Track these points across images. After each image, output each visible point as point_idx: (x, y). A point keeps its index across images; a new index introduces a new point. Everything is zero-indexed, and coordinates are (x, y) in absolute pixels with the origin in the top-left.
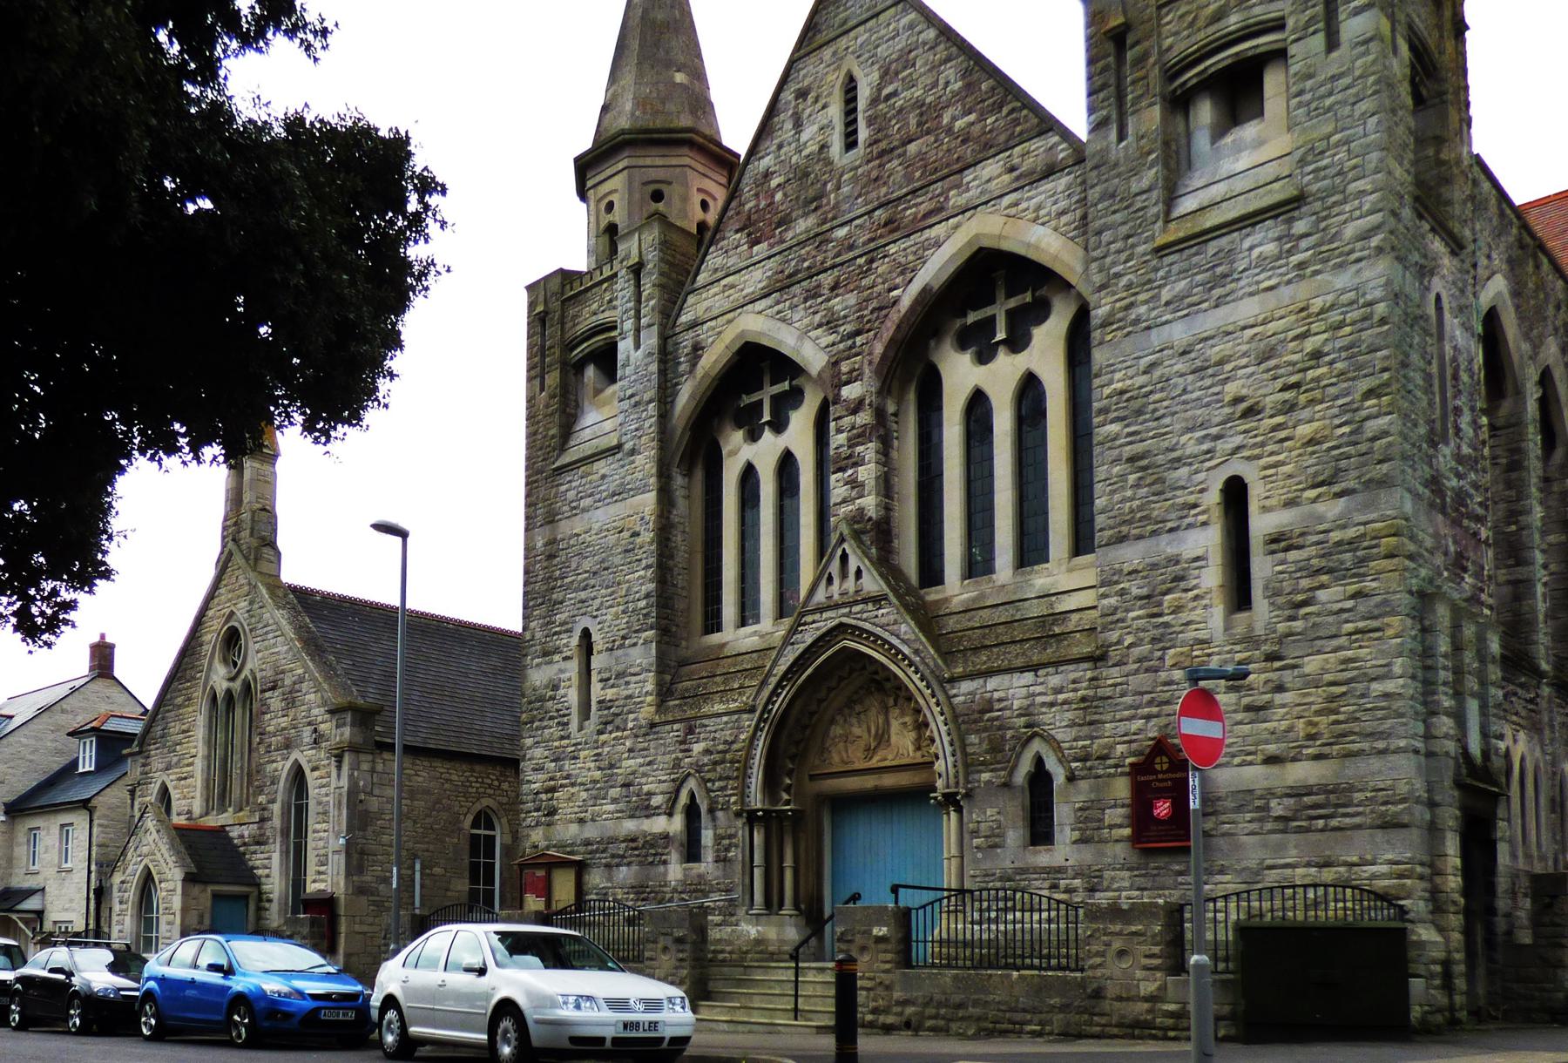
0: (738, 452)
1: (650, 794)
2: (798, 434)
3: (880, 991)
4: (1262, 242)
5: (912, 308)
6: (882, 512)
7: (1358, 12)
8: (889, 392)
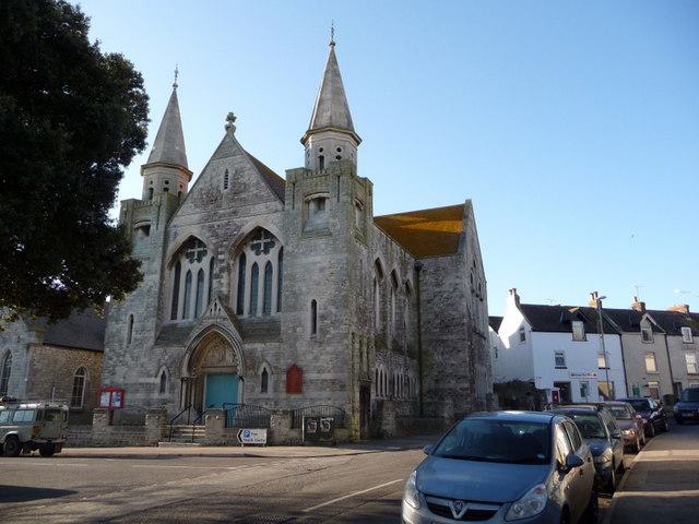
0: (186, 265)
2: (205, 263)
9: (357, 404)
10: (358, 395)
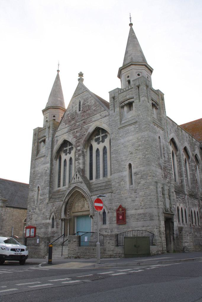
0: (64, 157)
1: (47, 216)
2: (72, 155)
3: (74, 251)
4: (132, 128)
5: (87, 136)
6: (83, 168)
7: (143, 97)
8: (85, 148)
9: (163, 229)
10: (163, 223)
